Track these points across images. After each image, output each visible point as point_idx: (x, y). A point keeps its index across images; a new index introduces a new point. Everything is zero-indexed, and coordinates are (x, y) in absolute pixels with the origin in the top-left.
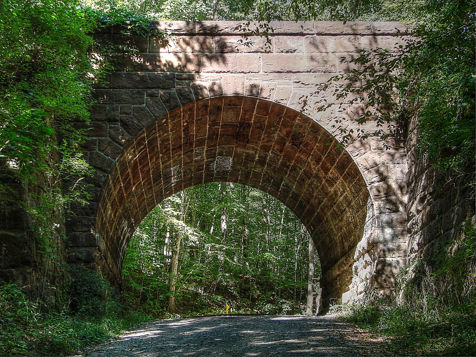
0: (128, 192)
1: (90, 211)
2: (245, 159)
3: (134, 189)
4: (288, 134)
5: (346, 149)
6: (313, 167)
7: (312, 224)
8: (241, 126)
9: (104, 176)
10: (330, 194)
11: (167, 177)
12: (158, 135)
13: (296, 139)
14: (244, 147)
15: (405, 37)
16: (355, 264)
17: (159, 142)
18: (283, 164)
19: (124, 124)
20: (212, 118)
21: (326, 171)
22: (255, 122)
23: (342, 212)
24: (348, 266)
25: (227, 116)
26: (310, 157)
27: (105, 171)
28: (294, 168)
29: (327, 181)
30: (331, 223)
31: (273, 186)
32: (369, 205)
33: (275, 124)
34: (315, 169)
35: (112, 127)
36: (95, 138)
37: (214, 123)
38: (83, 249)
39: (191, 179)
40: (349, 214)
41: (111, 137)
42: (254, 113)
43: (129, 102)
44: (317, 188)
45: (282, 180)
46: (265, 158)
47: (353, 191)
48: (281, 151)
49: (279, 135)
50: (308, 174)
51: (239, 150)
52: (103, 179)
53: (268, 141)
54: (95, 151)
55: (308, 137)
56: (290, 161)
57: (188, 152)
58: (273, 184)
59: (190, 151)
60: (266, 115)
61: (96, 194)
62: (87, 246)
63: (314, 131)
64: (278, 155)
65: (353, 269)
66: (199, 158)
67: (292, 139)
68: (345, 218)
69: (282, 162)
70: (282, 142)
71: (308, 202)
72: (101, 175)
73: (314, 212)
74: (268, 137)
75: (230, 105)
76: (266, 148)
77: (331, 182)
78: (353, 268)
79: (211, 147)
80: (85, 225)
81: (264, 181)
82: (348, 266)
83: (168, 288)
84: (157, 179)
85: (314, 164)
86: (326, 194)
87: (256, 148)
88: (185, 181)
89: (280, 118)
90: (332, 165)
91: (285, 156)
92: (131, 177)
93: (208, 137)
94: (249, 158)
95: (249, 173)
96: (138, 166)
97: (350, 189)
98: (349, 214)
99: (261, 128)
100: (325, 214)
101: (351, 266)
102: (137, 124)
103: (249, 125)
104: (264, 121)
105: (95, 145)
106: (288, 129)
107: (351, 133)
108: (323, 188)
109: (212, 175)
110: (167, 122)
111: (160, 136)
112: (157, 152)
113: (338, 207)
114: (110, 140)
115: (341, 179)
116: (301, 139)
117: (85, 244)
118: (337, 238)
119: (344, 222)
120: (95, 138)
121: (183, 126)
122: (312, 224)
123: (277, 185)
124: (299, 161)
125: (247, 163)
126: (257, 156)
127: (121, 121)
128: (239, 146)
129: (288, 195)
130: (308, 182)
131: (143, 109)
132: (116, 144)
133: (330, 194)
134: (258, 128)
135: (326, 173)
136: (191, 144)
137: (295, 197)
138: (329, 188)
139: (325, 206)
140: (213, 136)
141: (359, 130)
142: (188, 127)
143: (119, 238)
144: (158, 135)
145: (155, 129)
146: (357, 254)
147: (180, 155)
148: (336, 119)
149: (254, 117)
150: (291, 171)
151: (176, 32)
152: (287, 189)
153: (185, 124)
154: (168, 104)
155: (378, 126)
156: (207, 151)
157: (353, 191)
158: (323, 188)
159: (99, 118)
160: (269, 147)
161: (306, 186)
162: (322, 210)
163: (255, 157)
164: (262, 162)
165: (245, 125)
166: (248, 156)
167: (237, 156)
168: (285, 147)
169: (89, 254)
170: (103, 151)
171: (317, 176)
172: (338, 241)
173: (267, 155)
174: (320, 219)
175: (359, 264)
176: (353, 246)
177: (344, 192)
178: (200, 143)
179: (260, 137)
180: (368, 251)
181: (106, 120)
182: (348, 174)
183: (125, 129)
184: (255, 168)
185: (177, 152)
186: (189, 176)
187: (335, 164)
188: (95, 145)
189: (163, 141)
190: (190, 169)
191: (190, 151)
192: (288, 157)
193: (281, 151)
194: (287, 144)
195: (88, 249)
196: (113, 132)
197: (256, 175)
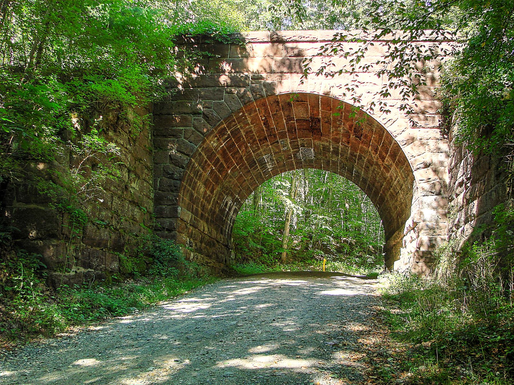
0: (224, 174)
1: (174, 188)
2: (323, 150)
3: (229, 171)
4: (351, 127)
5: (395, 139)
6: (373, 156)
7: (378, 203)
8: (312, 121)
9: (187, 159)
10: (387, 179)
11: (263, 164)
12: (239, 127)
13: (357, 131)
14: (320, 140)
15: (451, 43)
16: (405, 238)
17: (243, 134)
18: (352, 154)
19: (206, 116)
20: (286, 113)
21: (383, 159)
22: (323, 118)
23: (397, 194)
24: (400, 239)
25: (298, 112)
26: (370, 147)
27: (188, 155)
28: (360, 158)
29: (384, 167)
30: (390, 203)
31: (349, 173)
32: (415, 188)
33: (339, 119)
34: (375, 157)
35: (196, 119)
36: (181, 128)
37: (289, 118)
38: (168, 219)
39: (284, 165)
40: (401, 195)
41: (195, 127)
42: (320, 109)
43: (211, 99)
44: (378, 174)
45: (353, 168)
46: (338, 149)
47: (403, 176)
48: (348, 143)
49: (344, 129)
50: (370, 162)
51: (317, 142)
52: (186, 162)
53: (337, 134)
54: (181, 139)
55: (366, 130)
56: (356, 151)
57: (274, 143)
58: (348, 171)
59: (276, 142)
60: (330, 111)
61: (180, 174)
62: (171, 218)
63: (370, 123)
64: (346, 146)
65: (403, 243)
66: (286, 148)
67: (355, 132)
68: (399, 199)
69: (351, 152)
70: (347, 135)
71: (374, 185)
72: (185, 158)
73: (378, 193)
74: (336, 130)
75: (298, 101)
76: (337, 141)
77: (387, 168)
78: (403, 241)
79: (293, 140)
80: (170, 200)
81: (341, 168)
82: (400, 239)
83: (282, 246)
84: (252, 164)
85: (373, 153)
86: (385, 179)
87: (329, 140)
88: (280, 167)
89: (342, 113)
90: (387, 153)
91: (351, 147)
92: (222, 160)
93: (288, 131)
94: (326, 149)
95: (329, 161)
96: (227, 153)
97: (401, 174)
98: (401, 195)
99: (328, 122)
100: (386, 195)
101: (402, 239)
102: (216, 117)
103: (319, 120)
104: (330, 116)
105: (181, 133)
106: (349, 123)
107: (372, 106)
108: (382, 174)
109: (301, 163)
110: (243, 115)
111: (241, 128)
112: (244, 142)
113: (394, 190)
114: (194, 129)
115: (394, 166)
116: (361, 131)
117: (169, 216)
118: (394, 215)
119: (398, 203)
120: (181, 128)
121: (262, 120)
122: (378, 203)
123: (350, 171)
124: (362, 151)
125: (325, 154)
126: (331, 147)
127: (204, 114)
128: (315, 139)
129: (360, 179)
130: (371, 168)
131: (221, 104)
132: (198, 133)
133: (387, 179)
134: (326, 122)
135: (383, 161)
136: (275, 137)
137: (365, 181)
138: (386, 174)
139: (385, 189)
140: (291, 130)
141: (381, 103)
142: (267, 121)
143: (222, 211)
144: (239, 127)
145: (234, 121)
146: (406, 230)
147: (268, 145)
148: (347, 87)
149: (320, 112)
150: (358, 160)
151: (252, 41)
152: (358, 176)
153: (263, 118)
154: (242, 100)
155: (404, 99)
156: (290, 143)
157: (403, 176)
158: (382, 174)
159: (186, 111)
160: (338, 139)
161: (371, 172)
162: (384, 192)
163: (330, 149)
164: (336, 152)
165: (315, 120)
166: (324, 147)
167: (316, 147)
168: (350, 139)
169: (171, 224)
170: (187, 139)
171: (377, 164)
172: (395, 218)
173: (338, 147)
174: (382, 199)
175: (407, 238)
176: (404, 223)
177: (397, 177)
178: (283, 135)
179: (330, 131)
180: (413, 229)
181: (191, 113)
182: (399, 161)
183: (206, 120)
184: (332, 157)
185: (264, 143)
186: (282, 163)
187: (389, 153)
188: (181, 133)
189: (247, 133)
190: (281, 158)
191: (276, 142)
192: (354, 148)
193: (348, 143)
194: (351, 136)
195: (171, 220)
196: (196, 124)
197: (334, 163)
